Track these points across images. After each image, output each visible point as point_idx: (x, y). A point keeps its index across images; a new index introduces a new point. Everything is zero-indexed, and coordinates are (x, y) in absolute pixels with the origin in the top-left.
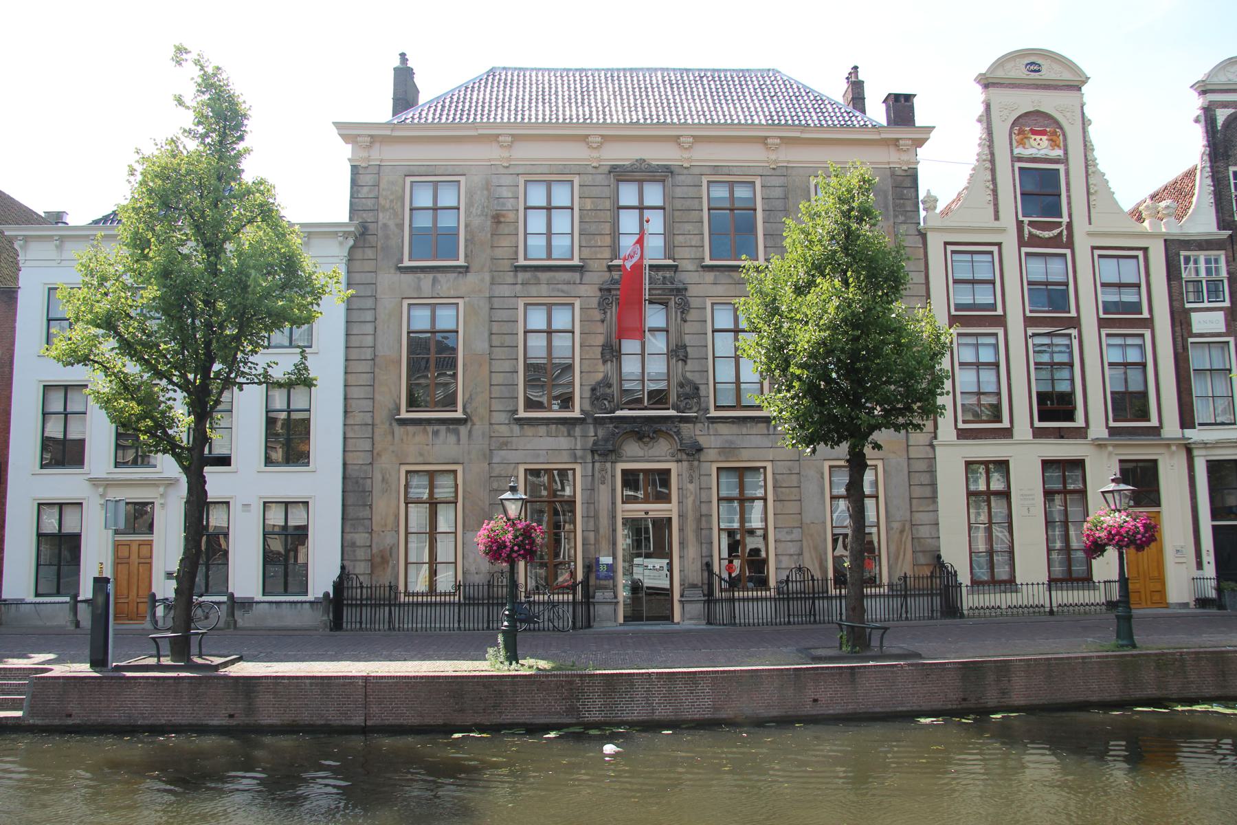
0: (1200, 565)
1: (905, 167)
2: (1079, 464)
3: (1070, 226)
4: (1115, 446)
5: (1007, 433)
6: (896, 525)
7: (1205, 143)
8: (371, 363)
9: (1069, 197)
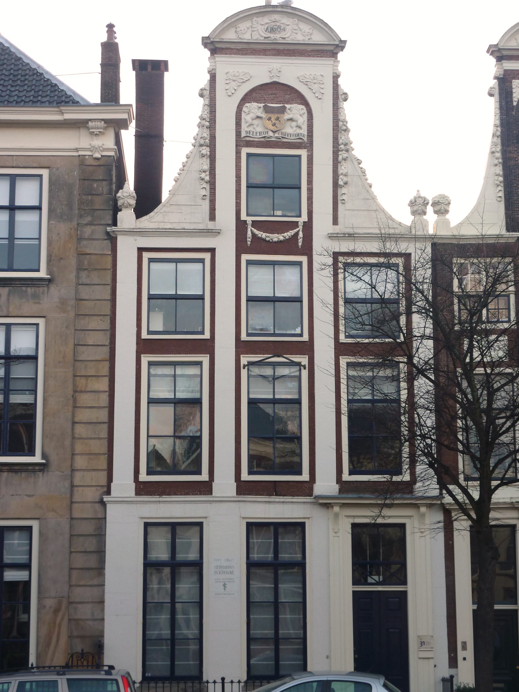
0: (453, 662)
1: (97, 155)
2: (298, 528)
3: (308, 226)
4: (344, 505)
5: (205, 488)
6: (50, 603)
7: (498, 122)
8: (77, 419)
9: (310, 190)
